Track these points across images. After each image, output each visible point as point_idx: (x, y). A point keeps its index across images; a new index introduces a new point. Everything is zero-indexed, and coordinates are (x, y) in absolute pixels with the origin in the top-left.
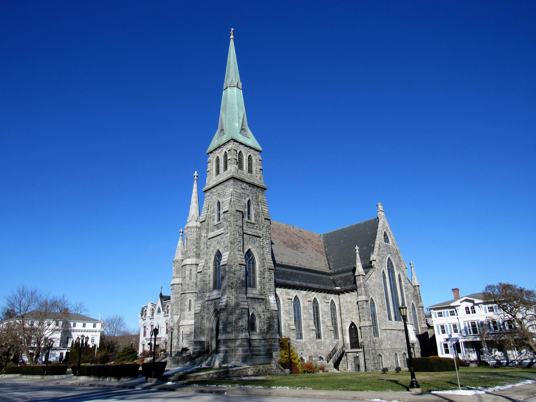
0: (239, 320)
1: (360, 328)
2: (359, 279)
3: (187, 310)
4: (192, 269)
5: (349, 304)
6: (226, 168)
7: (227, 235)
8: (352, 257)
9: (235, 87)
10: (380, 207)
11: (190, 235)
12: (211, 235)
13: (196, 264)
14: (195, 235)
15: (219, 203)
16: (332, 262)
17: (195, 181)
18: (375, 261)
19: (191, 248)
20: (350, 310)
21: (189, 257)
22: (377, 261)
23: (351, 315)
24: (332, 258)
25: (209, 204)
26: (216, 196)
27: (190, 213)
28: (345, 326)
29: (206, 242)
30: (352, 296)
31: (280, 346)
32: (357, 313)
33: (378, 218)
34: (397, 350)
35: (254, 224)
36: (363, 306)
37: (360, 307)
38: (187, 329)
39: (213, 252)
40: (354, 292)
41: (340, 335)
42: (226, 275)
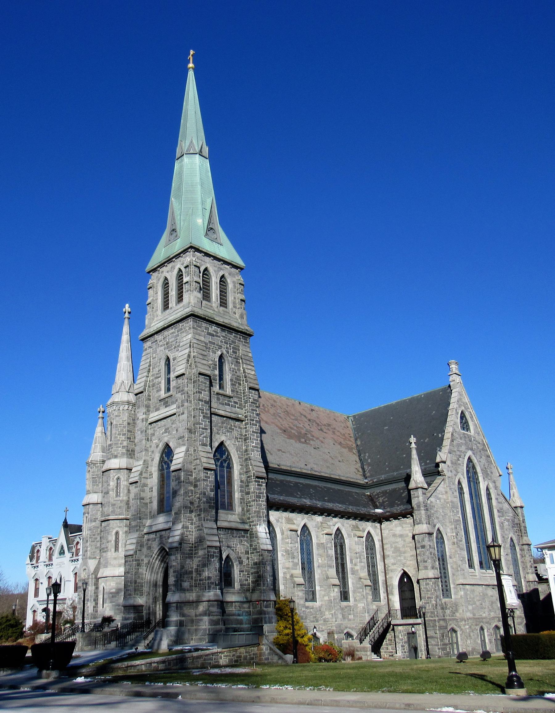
0: (203, 567)
1: (418, 582)
2: (416, 495)
3: (111, 550)
4: (121, 477)
5: (399, 540)
6: (180, 298)
7: (182, 417)
8: (404, 456)
9: (197, 154)
10: (454, 367)
11: (116, 416)
12: (154, 416)
13: (127, 469)
14: (125, 417)
15: (168, 359)
16: (369, 464)
17: (126, 321)
18: (444, 462)
19: (119, 440)
20: (401, 549)
21: (116, 457)
22: (448, 463)
23: (402, 558)
24: (369, 457)
25: (150, 362)
26: (162, 348)
27: (117, 379)
28: (391, 578)
29: (144, 429)
30: (404, 526)
31: (277, 614)
32: (412, 556)
33: (450, 386)
34: (484, 620)
35: (230, 397)
36: (424, 543)
37: (418, 545)
38: (112, 584)
39: (157, 446)
40: (407, 518)
41: (383, 595)
42: (180, 488)
